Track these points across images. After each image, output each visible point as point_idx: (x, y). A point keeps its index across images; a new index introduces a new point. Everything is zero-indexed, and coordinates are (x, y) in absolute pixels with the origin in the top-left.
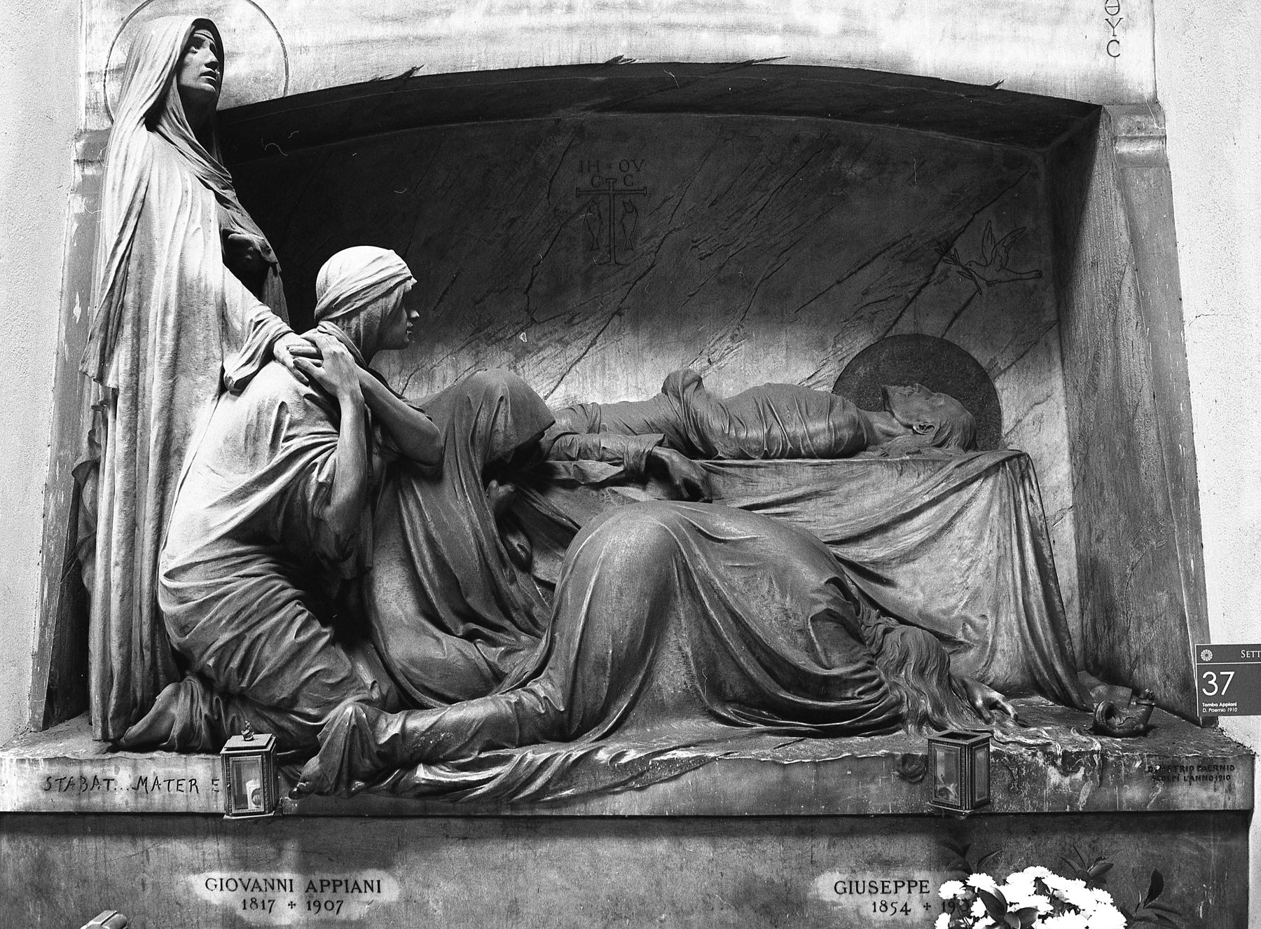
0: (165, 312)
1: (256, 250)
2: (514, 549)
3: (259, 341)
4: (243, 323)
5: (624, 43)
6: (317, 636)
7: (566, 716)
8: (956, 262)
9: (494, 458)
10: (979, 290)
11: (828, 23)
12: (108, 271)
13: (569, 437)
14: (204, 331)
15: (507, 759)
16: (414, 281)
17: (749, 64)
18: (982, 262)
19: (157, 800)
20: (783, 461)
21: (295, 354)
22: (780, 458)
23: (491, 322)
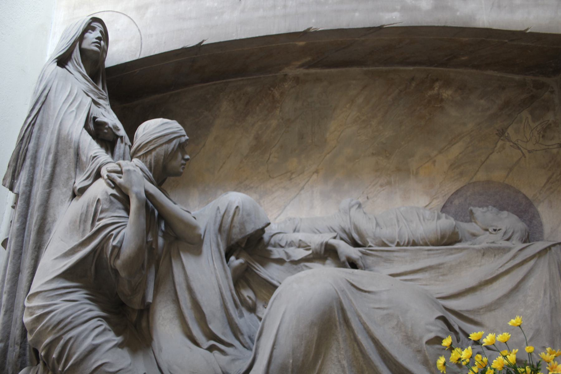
0: (49, 153)
1: (109, 128)
2: (245, 300)
3: (91, 168)
4: (87, 158)
6: (108, 341)
8: (509, 140)
9: (233, 242)
10: (524, 155)
13: (281, 235)
14: (67, 162)
16: (187, 137)
17: (381, 28)
18: (525, 140)
20: (409, 248)
23: (247, 178)
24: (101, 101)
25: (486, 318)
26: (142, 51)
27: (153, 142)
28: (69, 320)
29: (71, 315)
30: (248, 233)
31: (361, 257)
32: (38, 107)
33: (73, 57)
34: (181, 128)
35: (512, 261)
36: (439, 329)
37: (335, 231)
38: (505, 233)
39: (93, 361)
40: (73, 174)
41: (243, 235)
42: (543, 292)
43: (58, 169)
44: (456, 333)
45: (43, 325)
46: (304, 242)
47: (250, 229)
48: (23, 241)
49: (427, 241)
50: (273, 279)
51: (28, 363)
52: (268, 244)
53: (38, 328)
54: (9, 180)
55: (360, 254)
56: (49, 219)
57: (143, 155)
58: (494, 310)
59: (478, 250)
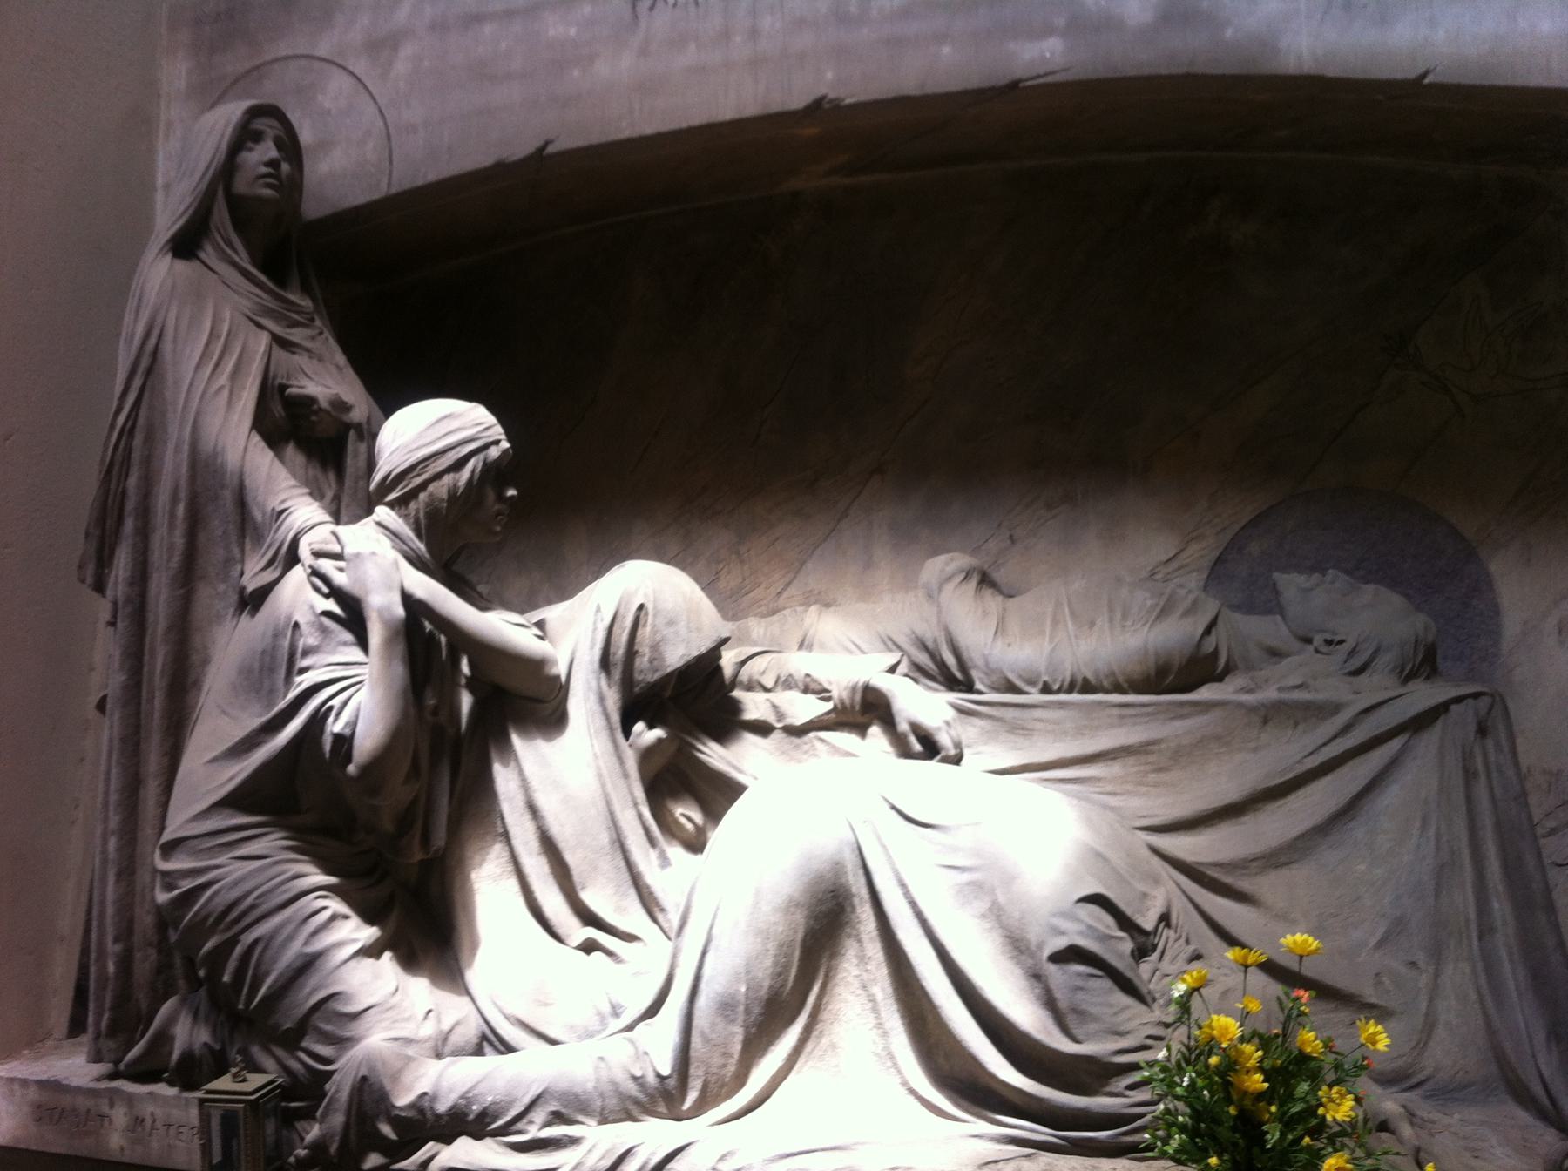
0: (175, 500)
1: (320, 409)
5: (829, 75)
7: (672, 1083)
9: (637, 689)
12: (105, 450)
17: (1014, 85)
24: (296, 335)
30: (669, 670)
31: (948, 723)
32: (137, 383)
34: (490, 419)
35: (1339, 740)
36: (1082, 927)
37: (899, 648)
38: (1353, 652)
39: (307, 990)
40: (236, 551)
41: (657, 676)
42: (1418, 824)
43: (202, 538)
45: (196, 914)
46: (814, 681)
47: (676, 656)
48: (138, 713)
49: (1121, 679)
50: (740, 771)
51: (181, 983)
54: (90, 569)
55: (951, 714)
56: (195, 658)
57: (397, 499)
58: (1287, 864)
59: (1252, 709)
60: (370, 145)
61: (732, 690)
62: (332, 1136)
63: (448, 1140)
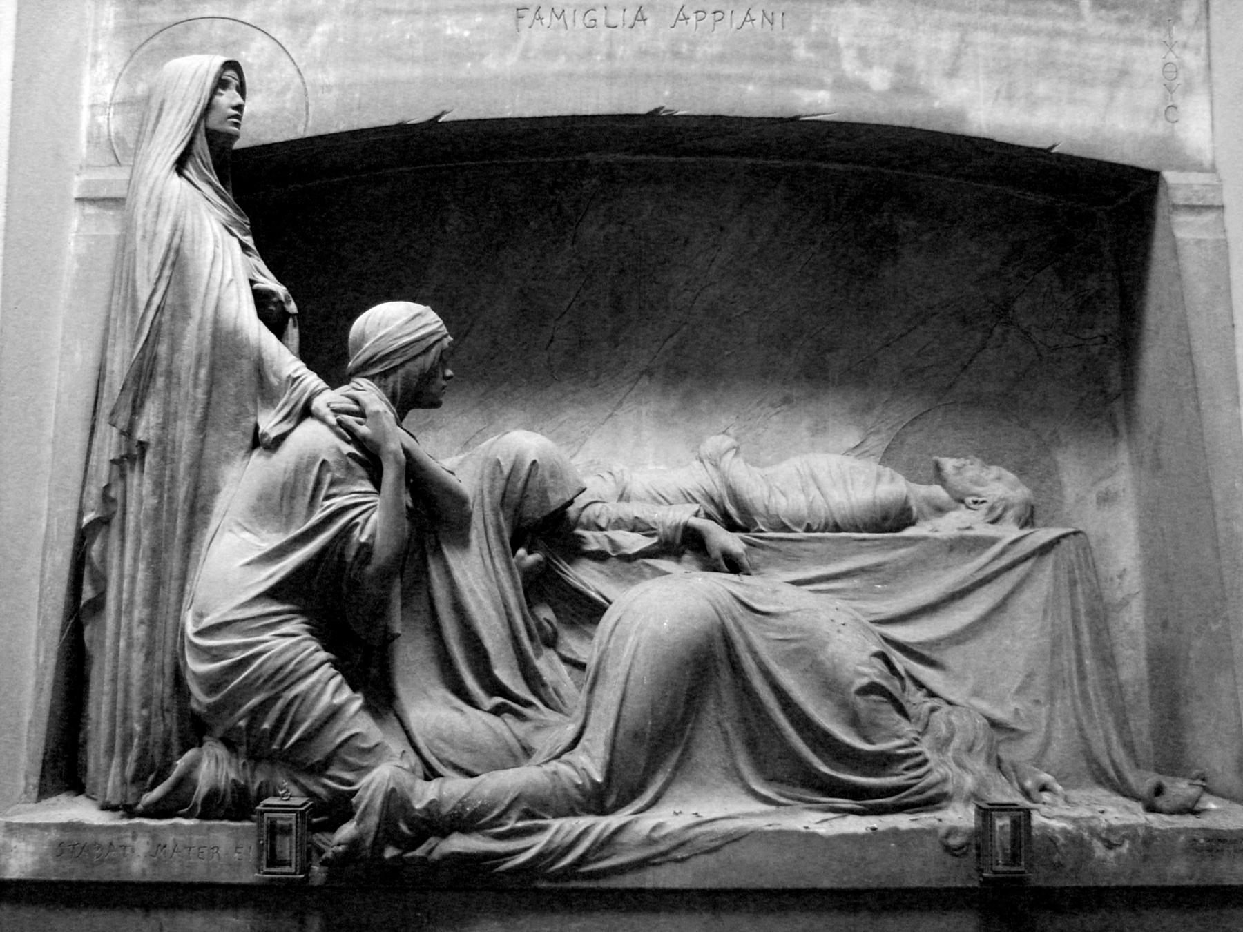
1: (280, 301)
7: (604, 788)
11: (879, 79)
15: (542, 829)
17: (795, 119)
19: (174, 872)
20: (827, 534)
21: (336, 411)
22: (823, 531)
25: (951, 657)
26: (310, 123)
27: (399, 354)
28: (291, 667)
29: (292, 659)
32: (167, 273)
33: (195, 151)
38: (992, 509)
44: (901, 679)
47: (556, 500)
52: (577, 523)
53: (236, 682)
57: (380, 374)
60: (289, 96)
61: (574, 528)
62: (367, 834)
63: (444, 835)
